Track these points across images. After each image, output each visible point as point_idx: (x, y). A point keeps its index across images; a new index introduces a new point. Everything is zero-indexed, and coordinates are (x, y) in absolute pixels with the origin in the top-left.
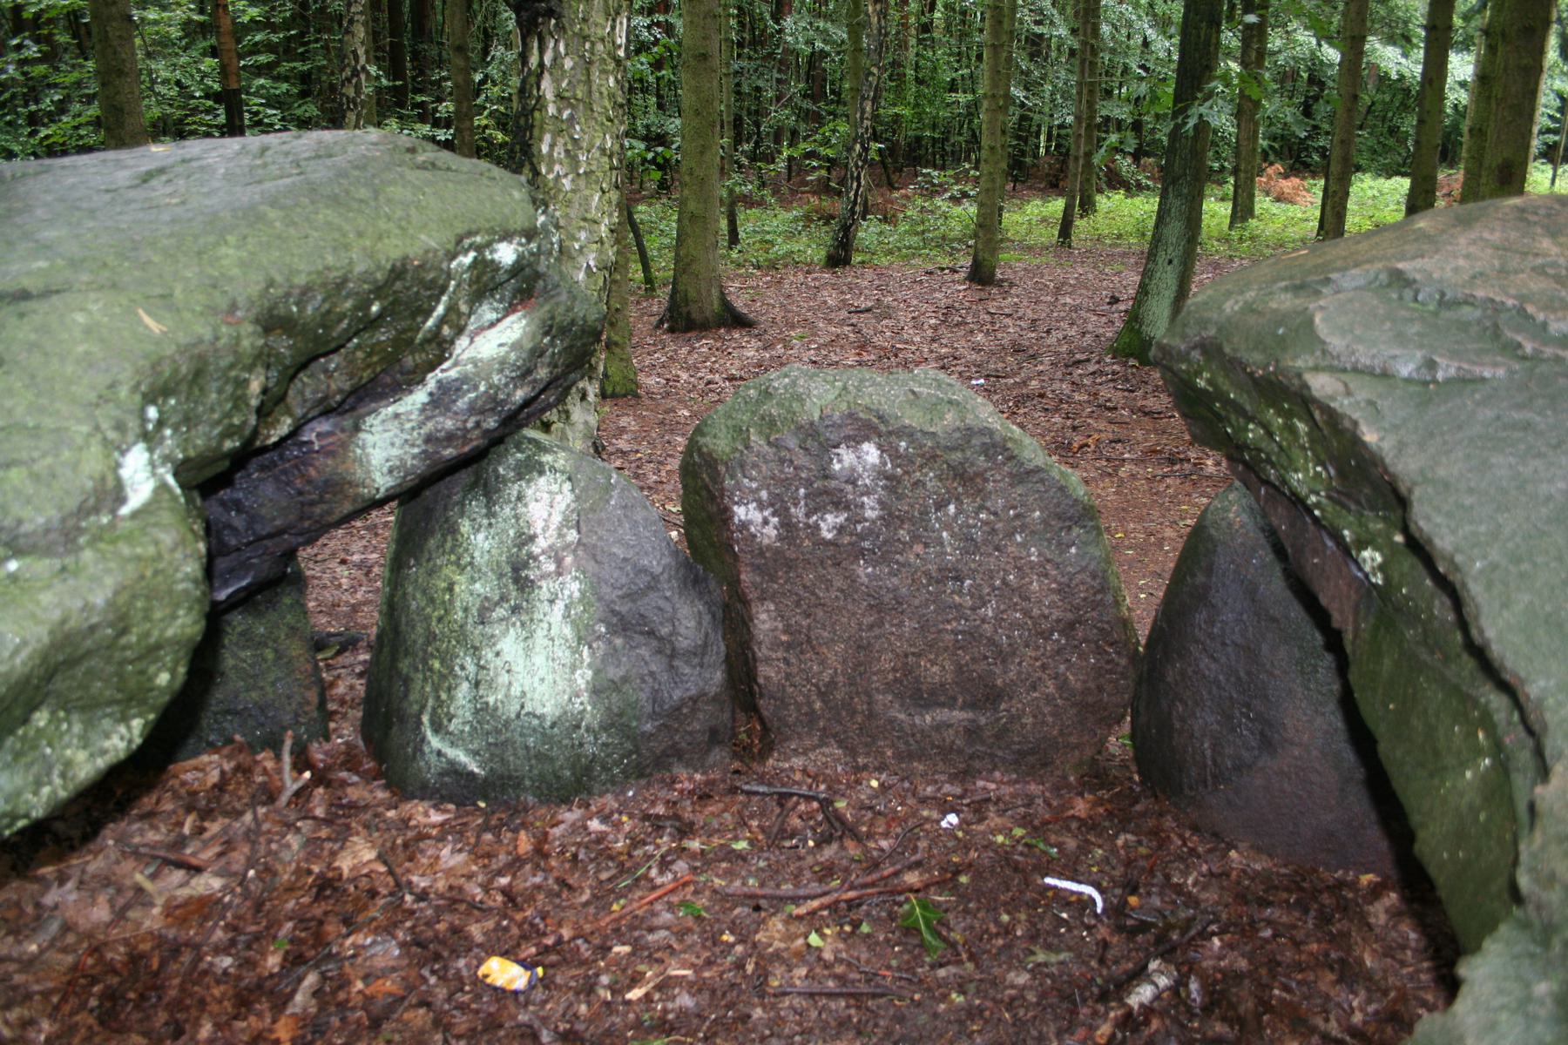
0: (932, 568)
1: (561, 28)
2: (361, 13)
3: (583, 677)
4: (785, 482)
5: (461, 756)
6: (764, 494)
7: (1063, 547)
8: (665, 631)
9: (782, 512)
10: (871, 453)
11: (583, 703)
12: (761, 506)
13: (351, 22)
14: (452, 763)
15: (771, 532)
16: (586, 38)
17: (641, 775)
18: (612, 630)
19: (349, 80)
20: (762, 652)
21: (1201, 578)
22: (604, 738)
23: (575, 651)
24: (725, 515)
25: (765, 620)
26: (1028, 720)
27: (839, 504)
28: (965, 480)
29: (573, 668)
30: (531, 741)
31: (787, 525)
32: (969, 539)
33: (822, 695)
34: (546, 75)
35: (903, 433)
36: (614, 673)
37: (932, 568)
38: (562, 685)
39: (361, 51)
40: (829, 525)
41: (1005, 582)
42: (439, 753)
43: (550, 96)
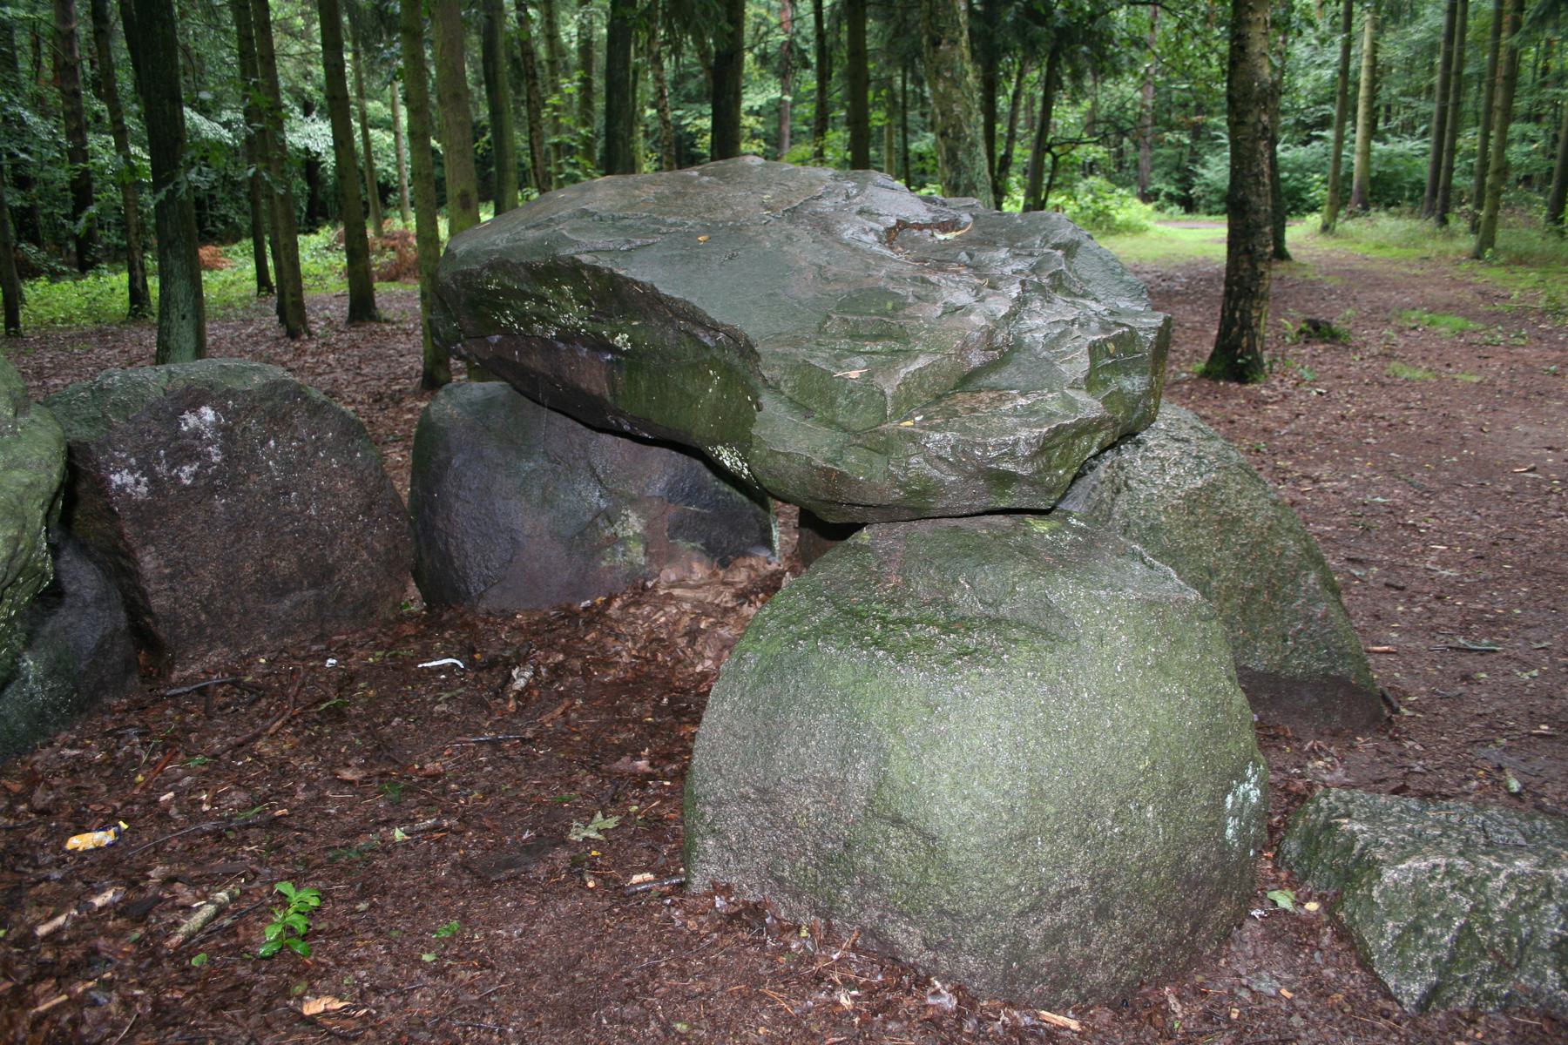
7: (352, 453)
10: (208, 414)
12: (132, 472)
15: (143, 489)
22: (49, 684)
25: (148, 562)
28: (278, 420)
31: (154, 481)
32: (288, 462)
33: (205, 608)
40: (186, 473)
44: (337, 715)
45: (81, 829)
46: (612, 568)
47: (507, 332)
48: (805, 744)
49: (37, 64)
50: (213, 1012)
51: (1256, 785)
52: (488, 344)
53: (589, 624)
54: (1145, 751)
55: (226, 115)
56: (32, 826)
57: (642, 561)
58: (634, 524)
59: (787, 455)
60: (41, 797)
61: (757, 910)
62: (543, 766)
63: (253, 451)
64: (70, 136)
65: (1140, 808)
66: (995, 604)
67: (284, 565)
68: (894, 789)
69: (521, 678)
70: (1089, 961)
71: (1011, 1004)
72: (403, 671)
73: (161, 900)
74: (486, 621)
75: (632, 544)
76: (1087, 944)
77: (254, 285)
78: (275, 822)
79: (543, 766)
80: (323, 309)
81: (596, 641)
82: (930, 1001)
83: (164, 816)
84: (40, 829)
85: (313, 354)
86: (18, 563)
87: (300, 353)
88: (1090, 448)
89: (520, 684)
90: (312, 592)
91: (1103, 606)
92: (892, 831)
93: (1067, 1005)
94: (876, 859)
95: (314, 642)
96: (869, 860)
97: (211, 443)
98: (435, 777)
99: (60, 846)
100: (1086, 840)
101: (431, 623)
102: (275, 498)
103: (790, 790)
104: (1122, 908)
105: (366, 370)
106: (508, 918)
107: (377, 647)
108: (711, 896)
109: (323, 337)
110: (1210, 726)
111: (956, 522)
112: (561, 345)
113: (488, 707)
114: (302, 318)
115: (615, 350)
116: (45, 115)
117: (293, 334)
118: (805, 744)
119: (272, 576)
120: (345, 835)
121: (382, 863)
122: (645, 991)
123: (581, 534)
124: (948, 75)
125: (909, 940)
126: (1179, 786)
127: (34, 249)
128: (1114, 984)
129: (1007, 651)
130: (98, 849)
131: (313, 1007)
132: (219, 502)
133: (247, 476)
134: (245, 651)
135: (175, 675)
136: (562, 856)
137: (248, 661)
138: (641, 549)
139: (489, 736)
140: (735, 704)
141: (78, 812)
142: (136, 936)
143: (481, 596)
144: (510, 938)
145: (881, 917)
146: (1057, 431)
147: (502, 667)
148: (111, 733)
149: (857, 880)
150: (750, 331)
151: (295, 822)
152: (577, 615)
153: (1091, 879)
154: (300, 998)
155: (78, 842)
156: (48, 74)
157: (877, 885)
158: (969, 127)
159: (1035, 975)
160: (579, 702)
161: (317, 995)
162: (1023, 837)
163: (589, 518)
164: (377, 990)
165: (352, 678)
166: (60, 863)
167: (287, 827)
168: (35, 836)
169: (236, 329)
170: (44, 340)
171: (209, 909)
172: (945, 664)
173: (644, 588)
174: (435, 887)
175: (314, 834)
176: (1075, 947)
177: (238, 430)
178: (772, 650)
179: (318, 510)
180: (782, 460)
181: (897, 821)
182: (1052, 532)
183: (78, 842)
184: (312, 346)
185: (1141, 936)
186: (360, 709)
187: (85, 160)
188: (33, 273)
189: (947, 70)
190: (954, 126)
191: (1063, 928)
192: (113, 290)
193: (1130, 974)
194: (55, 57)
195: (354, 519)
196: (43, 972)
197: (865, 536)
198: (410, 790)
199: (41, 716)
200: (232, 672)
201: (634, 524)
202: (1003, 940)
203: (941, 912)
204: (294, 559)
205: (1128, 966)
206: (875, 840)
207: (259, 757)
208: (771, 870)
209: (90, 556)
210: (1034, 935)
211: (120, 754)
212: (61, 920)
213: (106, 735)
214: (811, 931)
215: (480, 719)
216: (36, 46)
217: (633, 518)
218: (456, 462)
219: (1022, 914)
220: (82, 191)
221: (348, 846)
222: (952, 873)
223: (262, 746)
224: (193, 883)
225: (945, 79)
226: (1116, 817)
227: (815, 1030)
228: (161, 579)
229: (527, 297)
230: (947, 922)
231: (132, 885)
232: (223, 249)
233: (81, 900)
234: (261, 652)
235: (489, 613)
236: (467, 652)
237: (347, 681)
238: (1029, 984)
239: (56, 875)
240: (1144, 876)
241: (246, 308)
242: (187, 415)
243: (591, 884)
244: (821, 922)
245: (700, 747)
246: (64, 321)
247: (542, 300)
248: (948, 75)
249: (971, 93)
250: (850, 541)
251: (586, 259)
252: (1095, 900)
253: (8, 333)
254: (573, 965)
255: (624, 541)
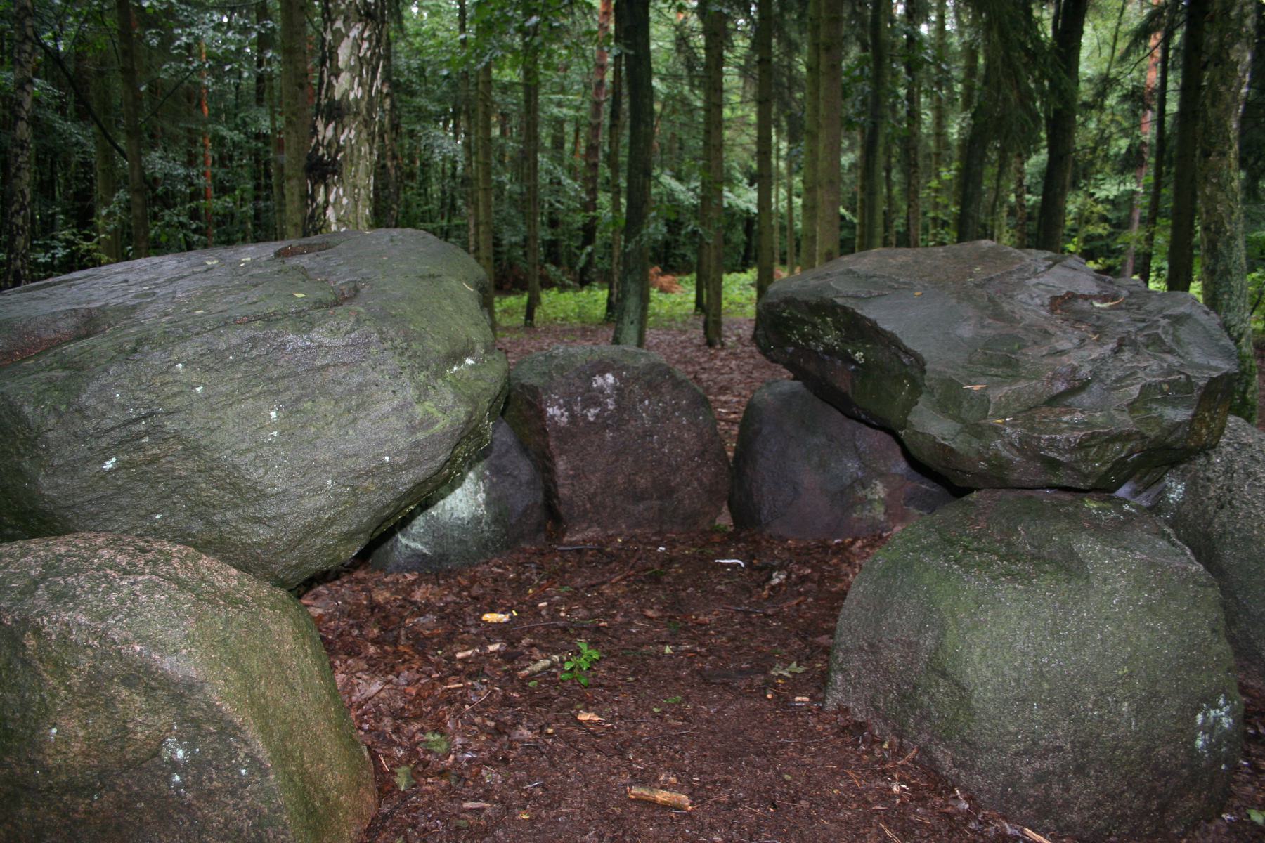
0: (640, 431)
1: (341, 180)
2: (27, 163)
3: (481, 497)
4: (571, 395)
5: (418, 546)
6: (561, 401)
7: (696, 417)
8: (516, 473)
9: (570, 410)
10: (610, 378)
11: (481, 511)
12: (560, 408)
13: (19, 169)
14: (413, 550)
15: (565, 420)
16: (355, 187)
17: (508, 548)
18: (492, 474)
19: (18, 212)
20: (560, 481)
21: (757, 426)
22: (493, 527)
23: (476, 484)
24: (544, 412)
25: (561, 465)
26: (687, 502)
27: (596, 403)
28: (652, 388)
29: (476, 493)
30: (456, 534)
31: (572, 416)
32: (655, 416)
33: (590, 499)
34: (330, 208)
35: (625, 368)
36: (494, 494)
37: (640, 431)
38: (471, 502)
39: (27, 191)
40: (592, 413)
41: (673, 435)
42: (407, 546)
43: (333, 219)
44: (656, 580)
45: (492, 611)
46: (860, 519)
47: (795, 344)
48: (900, 618)
49: (576, 143)
50: (531, 706)
51: (1228, 714)
52: (786, 353)
53: (835, 554)
54: (1125, 662)
55: (693, 184)
56: (468, 604)
57: (882, 517)
58: (879, 490)
59: (923, 434)
60: (476, 590)
61: (861, 727)
62: (772, 632)
63: (634, 405)
64: (588, 193)
65: (1116, 702)
66: (1040, 547)
67: (642, 482)
68: (945, 652)
69: (778, 578)
70: (1067, 805)
71: (1005, 818)
72: (705, 562)
73: (522, 654)
74: (768, 541)
75: (876, 504)
76: (1067, 789)
77: (693, 306)
78: (598, 629)
79: (772, 632)
80: (739, 328)
81: (835, 565)
82: (951, 802)
83: (538, 613)
84: (471, 607)
85: (722, 360)
86: (471, 426)
87: (713, 358)
88: (1121, 451)
89: (776, 581)
90: (658, 502)
91: (1112, 559)
92: (941, 680)
93: (1048, 830)
94: (930, 699)
95: (655, 534)
96: (926, 699)
97: (609, 396)
98: (702, 624)
99: (479, 618)
100: (1071, 714)
101: (733, 537)
102: (643, 438)
103: (887, 646)
104: (1096, 771)
105: (756, 374)
106: (712, 702)
107: (693, 546)
108: (836, 713)
109: (732, 347)
110: (1185, 658)
111: (1028, 493)
112: (827, 357)
113: (750, 592)
114: (719, 333)
115: (855, 362)
116: (575, 179)
117: (710, 344)
118: (900, 618)
119: (635, 487)
120: (637, 644)
121: (652, 662)
122: (774, 754)
123: (842, 492)
124: (1215, 181)
125: (944, 757)
126: (1154, 695)
127: (553, 268)
128: (1086, 827)
129: (1037, 577)
130: (499, 623)
131: (584, 717)
132: (609, 435)
133: (628, 421)
134: (610, 533)
135: (566, 539)
136: (759, 679)
137: (611, 539)
138: (882, 509)
139: (743, 608)
140: (865, 588)
141: (493, 602)
142: (505, 668)
143: (767, 524)
144: (708, 712)
145: (930, 740)
146: (1093, 436)
147: (768, 571)
148: (522, 564)
149: (918, 712)
150: (925, 355)
151: (610, 632)
152: (829, 547)
153: (1072, 742)
154: (578, 711)
155: (489, 617)
156: (582, 150)
157: (927, 717)
158: (1230, 223)
159: (1024, 802)
160: (810, 600)
161: (587, 711)
162: (1024, 700)
163: (848, 482)
164: (621, 718)
165: (671, 561)
166: (477, 626)
167: (606, 634)
168: (468, 610)
169: (674, 336)
170: (548, 331)
171: (547, 662)
172: (993, 579)
173: (880, 537)
174: (677, 679)
175: (619, 640)
176: (1057, 790)
177: (627, 392)
178: (894, 557)
179: (670, 450)
180: (920, 437)
181: (944, 674)
182: (1098, 509)
183: (489, 617)
184: (723, 354)
185: (1112, 797)
186: (670, 579)
187: (595, 209)
188: (548, 283)
189: (1214, 177)
190: (1216, 222)
191: (1047, 773)
192: (596, 301)
193: (1100, 823)
194: (587, 140)
195: (692, 459)
196: (456, 672)
197: (975, 495)
198: (686, 629)
199: (485, 546)
200: (600, 543)
201: (879, 490)
202: (1003, 768)
203: (963, 741)
204: (649, 479)
205: (1099, 817)
206: (931, 686)
207: (602, 594)
208: (873, 700)
209: (528, 455)
210: (1026, 771)
211: (523, 577)
212: (470, 652)
213: (518, 564)
214: (890, 745)
215: (743, 598)
216: (577, 131)
217: (880, 487)
218: (765, 432)
219: (1017, 754)
220: (588, 232)
221: (635, 650)
222: (971, 712)
223: (606, 589)
224: (542, 649)
225: (1213, 184)
226: (1096, 703)
227: (870, 799)
228: (568, 476)
229: (806, 323)
230: (966, 749)
231: (511, 644)
232: (677, 278)
233: (483, 646)
234: (620, 535)
235: (771, 537)
236: (749, 558)
237: (668, 561)
238: (1019, 807)
239: (473, 631)
240: (1117, 753)
241: (684, 322)
242: (597, 378)
243: (769, 696)
244: (896, 741)
245: (844, 612)
246: (563, 319)
247: (814, 326)
248: (1215, 181)
249: (1235, 196)
250: (965, 498)
251: (840, 301)
252: (1075, 759)
253: (526, 325)
254: (740, 733)
255: (871, 501)
